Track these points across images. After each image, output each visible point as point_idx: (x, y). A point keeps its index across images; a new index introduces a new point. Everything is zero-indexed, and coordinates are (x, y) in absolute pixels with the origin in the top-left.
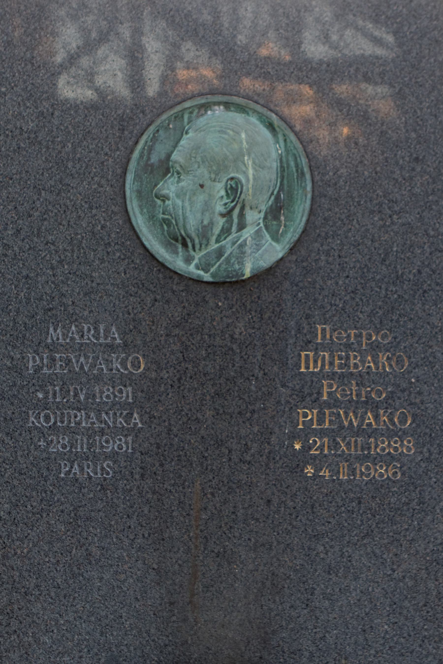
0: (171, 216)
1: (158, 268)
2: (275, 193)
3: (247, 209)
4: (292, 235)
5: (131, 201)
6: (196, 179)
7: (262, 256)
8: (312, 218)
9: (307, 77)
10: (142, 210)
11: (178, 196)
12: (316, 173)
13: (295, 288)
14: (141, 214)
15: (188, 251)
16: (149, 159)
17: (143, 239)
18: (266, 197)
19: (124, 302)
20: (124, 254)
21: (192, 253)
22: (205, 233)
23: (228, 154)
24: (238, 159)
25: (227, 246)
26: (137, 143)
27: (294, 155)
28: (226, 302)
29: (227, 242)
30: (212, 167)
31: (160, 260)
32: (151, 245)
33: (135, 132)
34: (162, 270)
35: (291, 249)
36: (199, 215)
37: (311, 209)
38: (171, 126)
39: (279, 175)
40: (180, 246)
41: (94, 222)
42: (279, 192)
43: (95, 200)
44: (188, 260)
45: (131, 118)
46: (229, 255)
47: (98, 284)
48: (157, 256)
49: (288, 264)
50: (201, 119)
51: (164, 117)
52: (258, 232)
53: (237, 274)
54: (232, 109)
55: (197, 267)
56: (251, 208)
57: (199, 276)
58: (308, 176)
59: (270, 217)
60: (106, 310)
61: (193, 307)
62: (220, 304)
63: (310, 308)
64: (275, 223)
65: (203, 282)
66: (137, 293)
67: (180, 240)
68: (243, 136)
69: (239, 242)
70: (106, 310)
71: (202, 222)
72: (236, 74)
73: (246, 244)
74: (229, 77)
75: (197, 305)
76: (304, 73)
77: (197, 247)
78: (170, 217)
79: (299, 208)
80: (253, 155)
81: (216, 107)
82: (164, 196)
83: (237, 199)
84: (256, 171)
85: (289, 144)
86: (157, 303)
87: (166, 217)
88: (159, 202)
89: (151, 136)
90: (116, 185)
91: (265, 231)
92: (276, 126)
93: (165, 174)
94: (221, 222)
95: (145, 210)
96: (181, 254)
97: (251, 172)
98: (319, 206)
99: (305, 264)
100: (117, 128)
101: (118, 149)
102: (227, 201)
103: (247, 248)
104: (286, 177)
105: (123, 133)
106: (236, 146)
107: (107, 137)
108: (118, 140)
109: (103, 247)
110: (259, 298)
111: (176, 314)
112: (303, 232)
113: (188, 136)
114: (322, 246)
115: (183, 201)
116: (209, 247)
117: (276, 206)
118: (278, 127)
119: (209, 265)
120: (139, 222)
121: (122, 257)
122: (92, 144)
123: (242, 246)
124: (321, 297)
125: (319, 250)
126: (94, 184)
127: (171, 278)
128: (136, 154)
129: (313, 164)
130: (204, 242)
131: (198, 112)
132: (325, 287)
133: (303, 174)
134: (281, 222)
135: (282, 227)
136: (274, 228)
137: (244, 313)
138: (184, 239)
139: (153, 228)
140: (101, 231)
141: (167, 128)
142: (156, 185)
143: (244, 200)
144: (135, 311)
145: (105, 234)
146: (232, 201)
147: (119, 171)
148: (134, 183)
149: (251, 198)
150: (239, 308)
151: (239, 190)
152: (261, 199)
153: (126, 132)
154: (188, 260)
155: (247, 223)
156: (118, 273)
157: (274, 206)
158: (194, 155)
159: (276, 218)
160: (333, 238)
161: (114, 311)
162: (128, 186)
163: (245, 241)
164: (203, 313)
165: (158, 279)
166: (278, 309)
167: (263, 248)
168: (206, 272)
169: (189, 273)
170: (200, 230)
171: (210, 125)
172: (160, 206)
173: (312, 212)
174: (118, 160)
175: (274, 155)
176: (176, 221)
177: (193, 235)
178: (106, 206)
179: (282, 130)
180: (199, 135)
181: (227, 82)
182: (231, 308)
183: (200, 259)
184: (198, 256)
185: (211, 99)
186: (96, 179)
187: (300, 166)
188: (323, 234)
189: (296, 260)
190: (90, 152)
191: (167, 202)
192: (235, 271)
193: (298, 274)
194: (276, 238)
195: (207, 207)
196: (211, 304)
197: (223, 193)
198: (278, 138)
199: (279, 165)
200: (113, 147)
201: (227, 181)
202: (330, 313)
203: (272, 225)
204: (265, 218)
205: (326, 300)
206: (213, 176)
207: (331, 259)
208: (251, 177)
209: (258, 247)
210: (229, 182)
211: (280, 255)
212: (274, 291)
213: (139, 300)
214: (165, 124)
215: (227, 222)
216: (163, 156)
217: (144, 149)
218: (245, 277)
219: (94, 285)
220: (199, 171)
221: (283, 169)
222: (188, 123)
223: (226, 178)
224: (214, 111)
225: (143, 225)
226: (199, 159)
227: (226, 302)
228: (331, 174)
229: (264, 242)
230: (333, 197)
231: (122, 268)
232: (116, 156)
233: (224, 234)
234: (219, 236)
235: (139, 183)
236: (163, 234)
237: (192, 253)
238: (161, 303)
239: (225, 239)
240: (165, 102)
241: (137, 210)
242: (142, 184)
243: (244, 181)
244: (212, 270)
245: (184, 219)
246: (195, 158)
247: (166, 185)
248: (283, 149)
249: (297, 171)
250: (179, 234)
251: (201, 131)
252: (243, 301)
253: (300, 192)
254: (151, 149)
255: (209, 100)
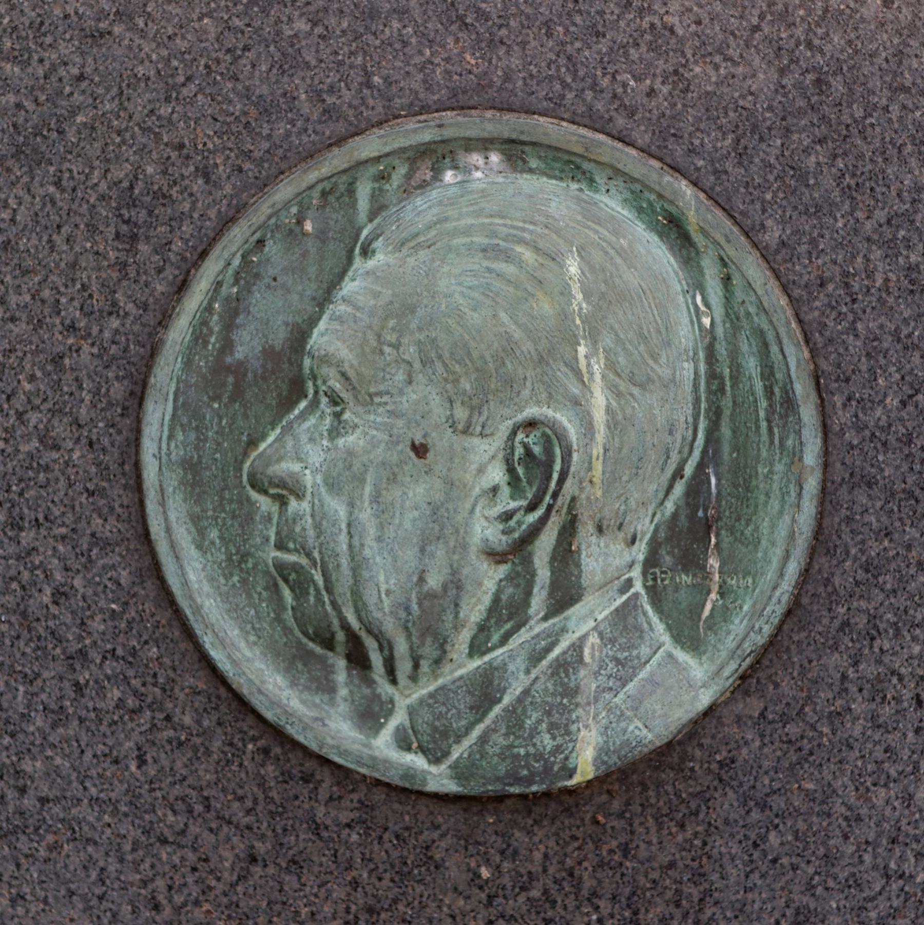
0: (308, 555)
1: (261, 743)
2: (689, 470)
3: (586, 534)
4: (747, 625)
5: (163, 503)
6: (400, 423)
7: (637, 702)
8: (822, 561)
9: (809, 45)
10: (201, 532)
11: (333, 485)
12: (838, 400)
13: (755, 815)
14: (199, 547)
15: (370, 683)
16: (227, 345)
17: (207, 641)
18: (653, 487)
19: (137, 864)
20: (135, 693)
21: (385, 688)
22: (430, 619)
23: (517, 334)
24: (552, 354)
25: (511, 667)
26: (182, 287)
27: (760, 334)
28: (506, 865)
29: (510, 653)
30: (456, 381)
31: (269, 715)
32: (234, 663)
33: (177, 245)
34: (278, 750)
35: (743, 678)
36: (409, 556)
37: (818, 530)
38: (308, 227)
39: (703, 405)
40: (341, 663)
41: (26, 575)
42: (701, 467)
43: (30, 494)
44: (371, 715)
45: (162, 196)
46: (520, 700)
47: (44, 800)
48: (257, 702)
49: (733, 731)
50: (419, 201)
51: (284, 191)
52: (624, 614)
53: (547, 769)
54: (533, 163)
55: (403, 742)
56: (600, 529)
57: (409, 773)
58: (808, 413)
59: (668, 560)
60: (72, 894)
61: (386, 882)
62: (485, 873)
63: (810, 887)
64: (686, 579)
65: (421, 794)
66: (183, 832)
67: (339, 644)
68: (573, 268)
69: (557, 651)
70: (72, 894)
71: (422, 580)
72: (549, 35)
73: (581, 660)
74: (524, 44)
75: (403, 875)
76: (799, 32)
77: (404, 667)
78: (304, 561)
79: (773, 526)
80: (608, 340)
81: (476, 158)
82: (282, 484)
83: (547, 499)
84: (619, 395)
85: (739, 294)
86: (257, 870)
87: (292, 558)
88: (264, 503)
89: (237, 262)
90: (106, 441)
91: (648, 608)
92: (692, 230)
93: (288, 403)
94: (490, 579)
95: (214, 534)
96: (343, 692)
97: (599, 400)
98: (849, 520)
99: (793, 730)
100: (110, 232)
101: (114, 310)
102: (513, 505)
103: (582, 673)
104: (727, 413)
105: (132, 250)
106: (545, 307)
107: (74, 265)
108: (115, 275)
109: (59, 667)
110: (625, 850)
111: (328, 909)
112: (789, 613)
113: (371, 263)
114: (856, 664)
115: (351, 505)
116: (447, 668)
117: (692, 517)
118: (702, 230)
119: (445, 734)
120: (192, 577)
121: (131, 702)
122: (18, 290)
123: (563, 667)
124: (850, 849)
125: (844, 677)
126: (27, 437)
127: (306, 779)
128: (180, 331)
129: (824, 365)
130: (429, 650)
131: (409, 176)
132: (864, 811)
133: (790, 403)
134: (707, 576)
135: (713, 596)
136: (684, 596)
137: (571, 903)
138: (354, 639)
139: (242, 600)
140: (54, 610)
141: (294, 234)
142: (253, 443)
143: (573, 499)
144: (178, 899)
145: (68, 618)
146: (531, 508)
147: (118, 390)
148: (171, 437)
149: (599, 493)
150: (553, 889)
151: (557, 467)
152: (635, 497)
153: (144, 248)
154: (371, 715)
155: (585, 582)
156: (116, 762)
157: (683, 521)
158: (391, 337)
159: (692, 562)
160: (898, 633)
161: (101, 898)
162: (149, 447)
163: (577, 647)
164: (423, 907)
165: (262, 783)
166: (695, 892)
167: (643, 674)
168: (436, 760)
169: (374, 762)
170: (415, 607)
171: (449, 226)
172: (269, 519)
173: (821, 541)
174: (114, 350)
175: (685, 335)
176: (325, 574)
177: (390, 626)
178: (69, 519)
179: (716, 243)
180: (411, 261)
181: (515, 62)
182: (523, 889)
183: (412, 712)
184: (405, 699)
185: (457, 125)
186: (33, 418)
187: (779, 376)
188: (861, 621)
189: (762, 715)
190: (13, 319)
191: (293, 505)
192: (539, 757)
193: (766, 764)
194: (689, 634)
195: (439, 525)
196: (454, 871)
197: (497, 474)
198: (701, 272)
199: (702, 367)
200: (98, 302)
201: (514, 433)
202: (883, 905)
203: (677, 589)
204: (651, 562)
205: (867, 858)
206: (461, 414)
207: (887, 710)
208: (599, 417)
209: (625, 668)
210: (520, 436)
211: (705, 699)
212: (682, 826)
213: (191, 856)
214: (288, 220)
215: (509, 578)
216: (279, 337)
217: (209, 309)
218: (576, 780)
219: (29, 802)
220: (412, 395)
221: (717, 382)
222: (372, 216)
223: (510, 423)
224: (467, 170)
225: (206, 588)
226: (410, 352)
227: (506, 865)
228: (892, 402)
229: (645, 650)
230: (899, 486)
231: (129, 744)
232: (107, 334)
233: (500, 622)
234: (483, 628)
235: (193, 436)
236: (278, 619)
237: (385, 688)
238: (271, 870)
239: (504, 640)
240: (288, 134)
241: (184, 535)
242: (201, 439)
243: (573, 433)
244: (456, 753)
245: (355, 571)
246: (396, 346)
247: (290, 444)
248: (719, 312)
249: (769, 392)
250: (336, 622)
251: (417, 248)
252: (569, 862)
253: (779, 467)
254: (234, 310)
255: (448, 133)
